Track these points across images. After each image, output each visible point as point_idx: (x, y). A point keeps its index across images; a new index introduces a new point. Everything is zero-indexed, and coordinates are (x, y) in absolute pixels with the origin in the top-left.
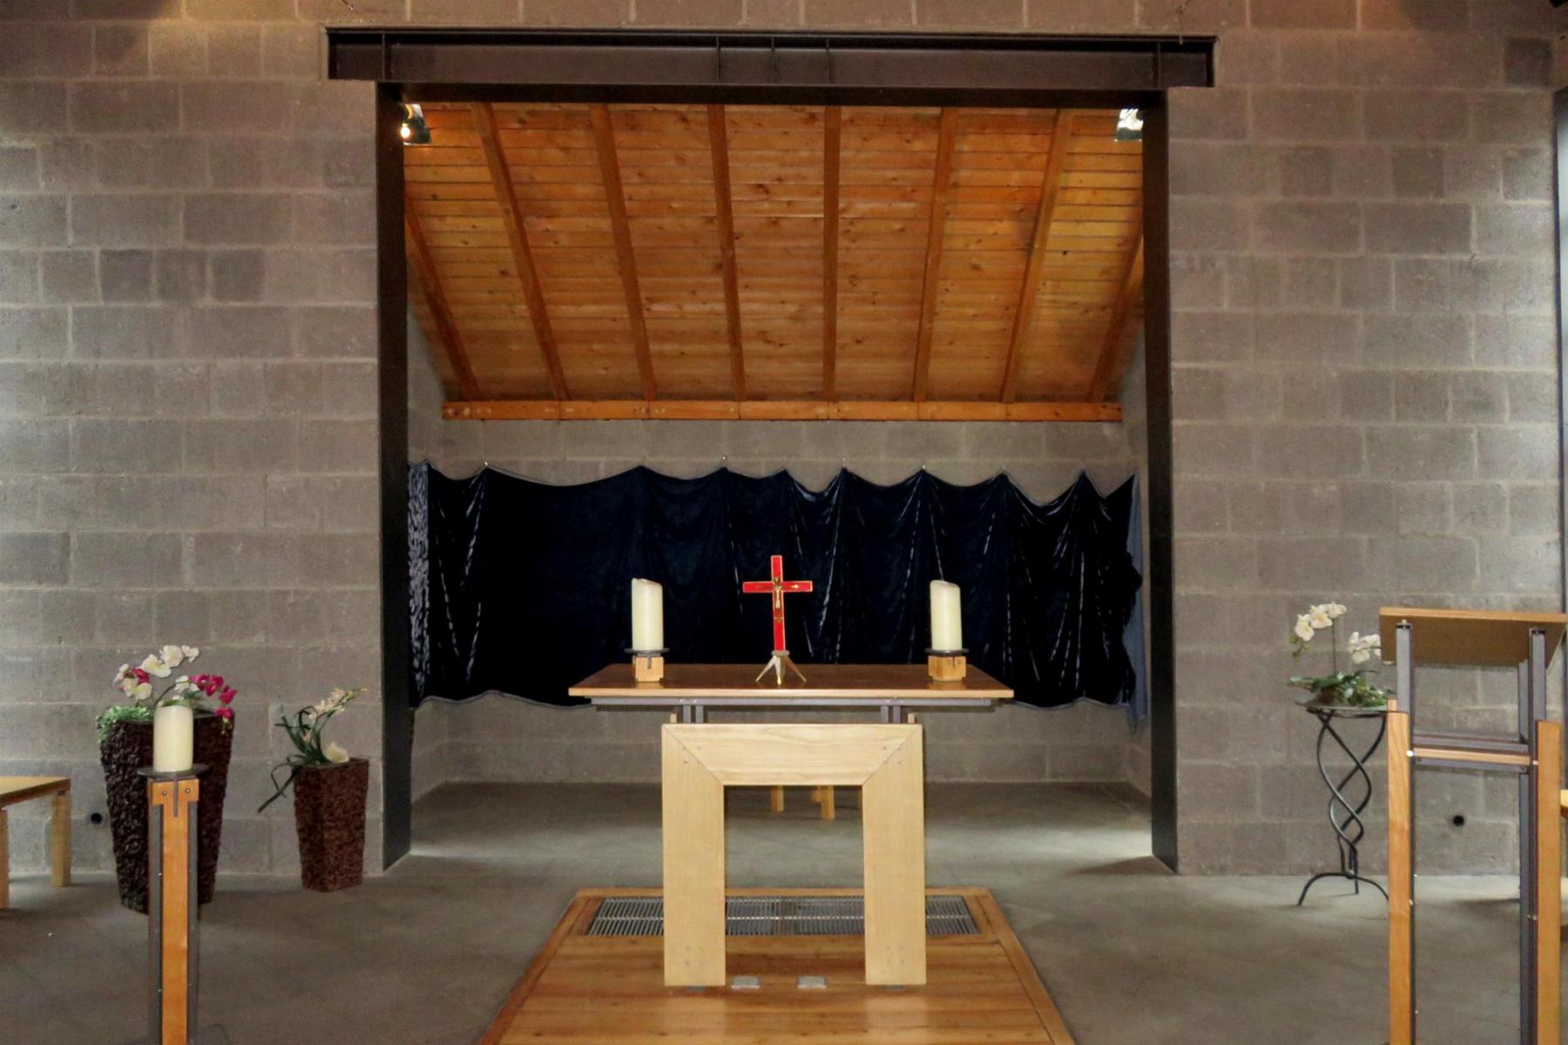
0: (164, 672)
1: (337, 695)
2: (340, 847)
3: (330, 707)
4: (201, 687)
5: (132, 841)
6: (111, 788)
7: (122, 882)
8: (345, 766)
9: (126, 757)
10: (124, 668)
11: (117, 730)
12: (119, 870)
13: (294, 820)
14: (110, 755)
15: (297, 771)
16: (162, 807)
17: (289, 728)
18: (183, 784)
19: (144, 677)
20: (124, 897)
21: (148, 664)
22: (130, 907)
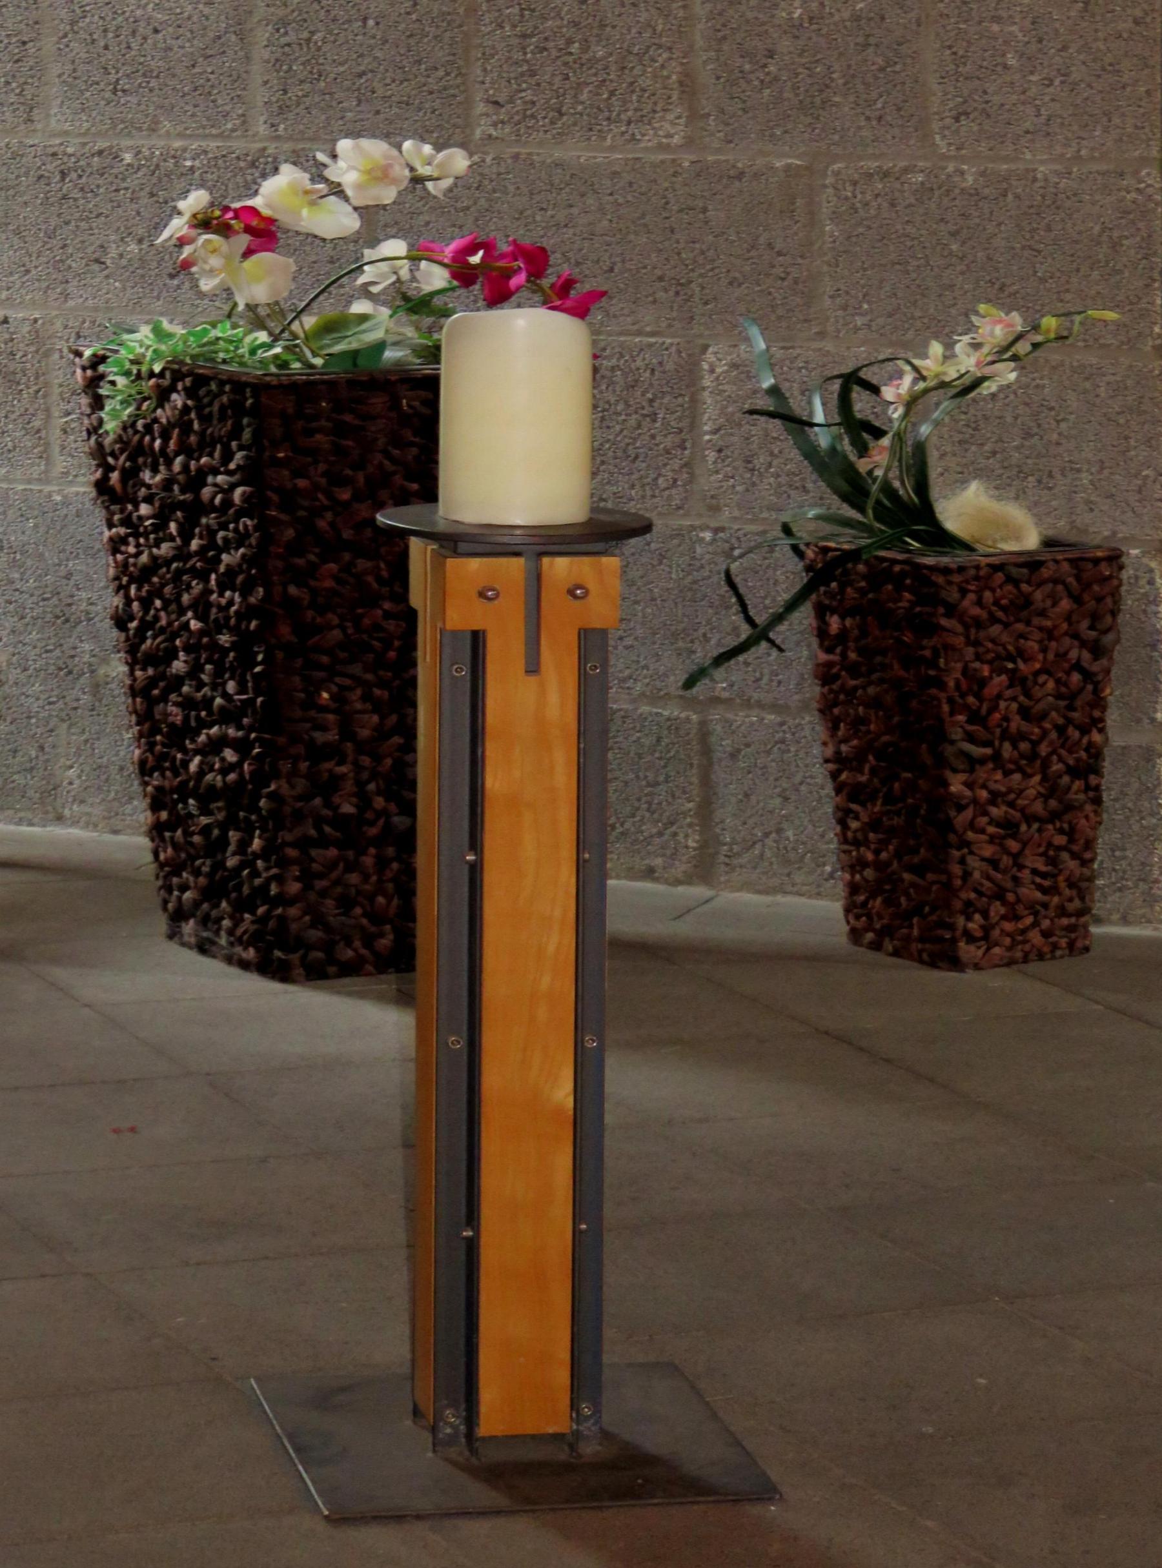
0: (336, 220)
1: (995, 326)
2: (1009, 827)
3: (967, 362)
4: (464, 275)
5: (215, 746)
6: (128, 577)
7: (169, 870)
8: (1031, 563)
9: (195, 482)
10: (195, 200)
11: (163, 396)
12: (157, 831)
13: (811, 729)
14: (130, 475)
15: (826, 574)
16: (477, 639)
17: (798, 424)
18: (559, 568)
19: (264, 233)
20: (178, 916)
21: (277, 192)
22: (203, 948)
